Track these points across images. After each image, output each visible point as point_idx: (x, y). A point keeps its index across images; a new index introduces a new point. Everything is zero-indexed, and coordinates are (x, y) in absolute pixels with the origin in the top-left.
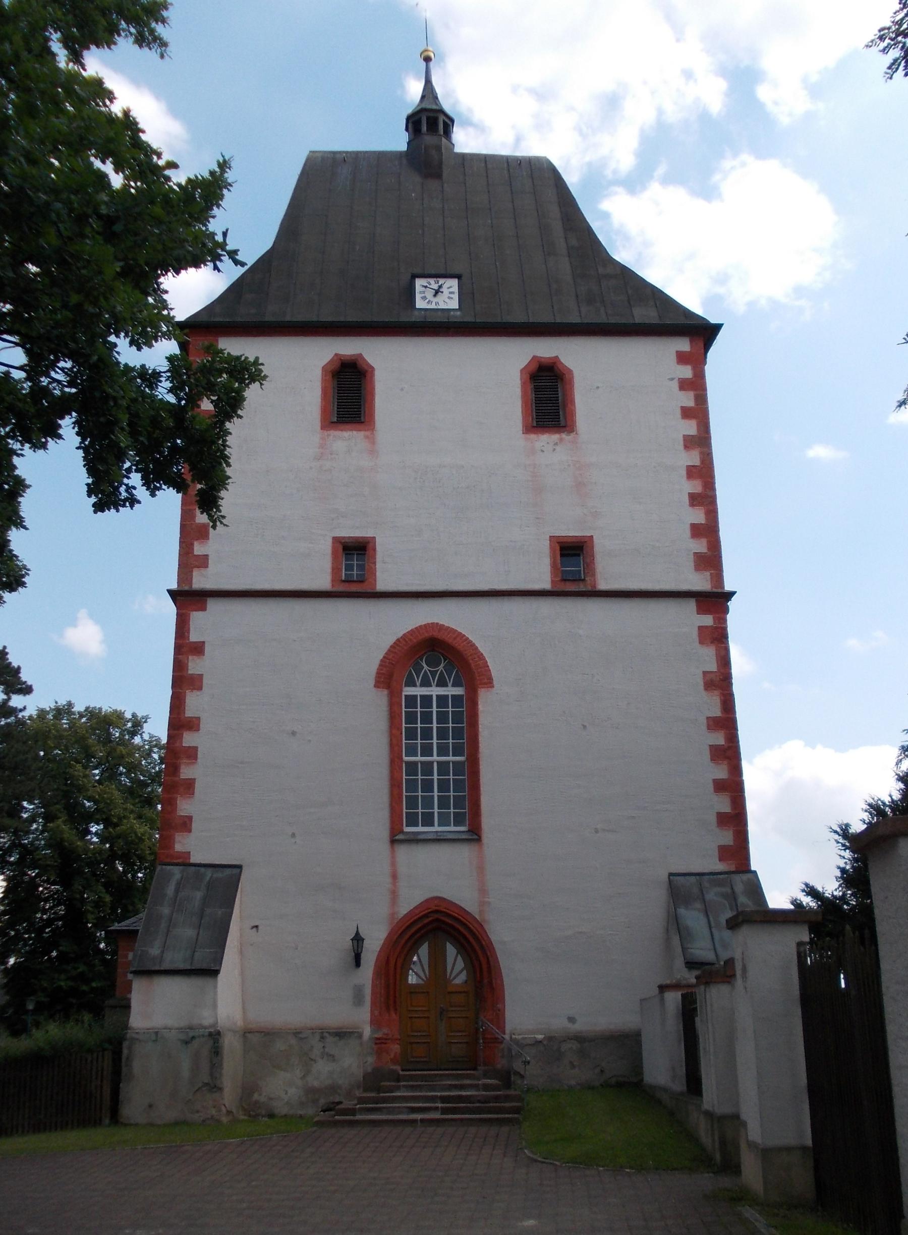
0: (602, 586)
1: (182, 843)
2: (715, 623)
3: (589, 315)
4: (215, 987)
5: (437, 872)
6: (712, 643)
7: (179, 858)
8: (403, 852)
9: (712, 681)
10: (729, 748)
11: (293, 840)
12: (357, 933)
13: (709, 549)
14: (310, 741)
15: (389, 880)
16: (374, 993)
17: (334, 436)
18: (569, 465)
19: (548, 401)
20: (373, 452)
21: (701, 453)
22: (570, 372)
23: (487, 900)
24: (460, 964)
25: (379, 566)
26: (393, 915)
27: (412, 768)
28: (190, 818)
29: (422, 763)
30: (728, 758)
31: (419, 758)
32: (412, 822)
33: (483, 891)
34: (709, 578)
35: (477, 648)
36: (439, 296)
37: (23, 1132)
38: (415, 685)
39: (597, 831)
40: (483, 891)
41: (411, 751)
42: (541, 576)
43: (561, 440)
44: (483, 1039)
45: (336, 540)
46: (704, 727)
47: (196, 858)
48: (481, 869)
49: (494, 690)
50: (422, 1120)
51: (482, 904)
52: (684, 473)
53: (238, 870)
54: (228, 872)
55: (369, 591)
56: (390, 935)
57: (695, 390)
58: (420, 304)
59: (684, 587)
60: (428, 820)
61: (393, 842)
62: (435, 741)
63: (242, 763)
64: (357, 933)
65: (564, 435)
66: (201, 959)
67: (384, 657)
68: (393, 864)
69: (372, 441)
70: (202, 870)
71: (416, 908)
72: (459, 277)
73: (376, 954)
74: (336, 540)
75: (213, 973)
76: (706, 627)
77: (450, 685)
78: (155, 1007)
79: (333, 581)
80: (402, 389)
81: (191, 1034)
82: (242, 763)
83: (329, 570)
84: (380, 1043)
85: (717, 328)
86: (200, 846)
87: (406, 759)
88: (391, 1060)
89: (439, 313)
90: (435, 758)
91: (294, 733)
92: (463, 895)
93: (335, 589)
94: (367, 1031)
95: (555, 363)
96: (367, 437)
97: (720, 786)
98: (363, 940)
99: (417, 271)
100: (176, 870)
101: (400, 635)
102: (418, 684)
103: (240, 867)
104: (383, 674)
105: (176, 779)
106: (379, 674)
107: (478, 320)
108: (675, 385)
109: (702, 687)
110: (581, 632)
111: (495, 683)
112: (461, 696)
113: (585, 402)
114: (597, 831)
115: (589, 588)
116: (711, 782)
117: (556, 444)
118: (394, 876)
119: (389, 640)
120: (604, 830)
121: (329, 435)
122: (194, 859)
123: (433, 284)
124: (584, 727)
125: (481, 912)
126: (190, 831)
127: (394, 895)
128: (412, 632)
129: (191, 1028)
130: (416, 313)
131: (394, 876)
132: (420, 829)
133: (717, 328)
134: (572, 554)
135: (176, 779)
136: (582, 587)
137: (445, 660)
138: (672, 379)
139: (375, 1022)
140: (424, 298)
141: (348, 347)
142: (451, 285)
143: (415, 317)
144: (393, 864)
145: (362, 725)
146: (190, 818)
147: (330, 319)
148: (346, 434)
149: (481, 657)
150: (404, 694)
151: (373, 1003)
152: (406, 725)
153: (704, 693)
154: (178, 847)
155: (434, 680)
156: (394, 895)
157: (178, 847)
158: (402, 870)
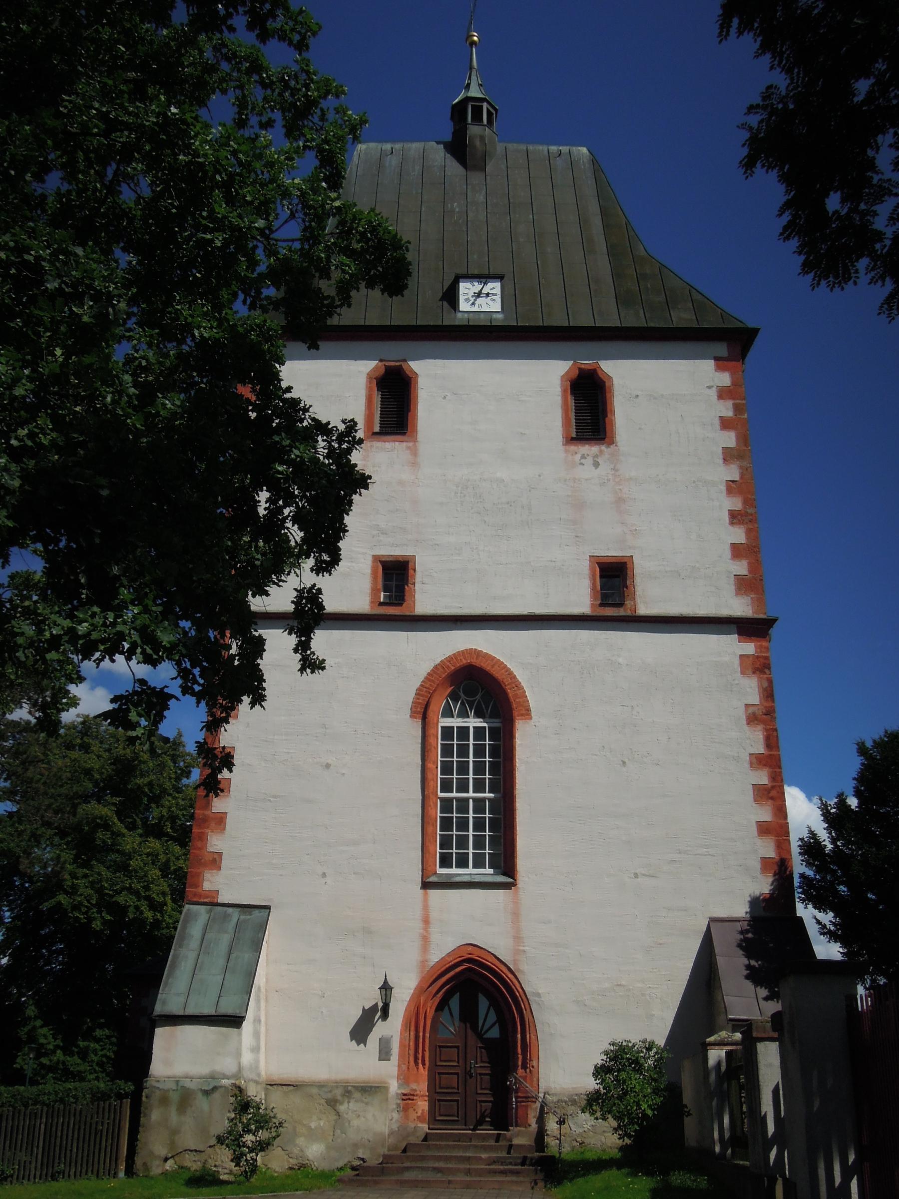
0: (643, 610)
1: (211, 881)
2: (756, 652)
3: (634, 319)
4: (240, 1034)
5: (471, 919)
6: (754, 673)
7: (207, 897)
8: (434, 893)
9: (754, 714)
10: (773, 787)
11: (323, 881)
12: (386, 982)
13: (750, 572)
14: (343, 774)
15: (421, 925)
16: (402, 1045)
17: (377, 447)
18: (609, 480)
19: (590, 413)
20: (414, 464)
21: (741, 467)
22: (610, 378)
23: (521, 948)
24: (492, 1017)
25: (418, 587)
26: (424, 962)
27: (447, 805)
28: (220, 854)
29: (475, 800)
30: (772, 798)
31: (454, 794)
32: (445, 861)
33: (518, 938)
34: (750, 602)
35: (515, 677)
36: (481, 300)
37: (35, 1182)
38: (453, 717)
39: (636, 876)
40: (518, 938)
41: (446, 786)
42: (580, 598)
43: (601, 452)
44: (516, 1098)
45: (376, 558)
46: (747, 765)
47: (224, 897)
48: (516, 915)
49: (532, 722)
50: (509, 1182)
51: (517, 952)
52: (723, 488)
53: (264, 913)
54: (256, 913)
55: (408, 613)
56: (421, 981)
57: (733, 399)
58: (464, 306)
59: (724, 612)
60: (462, 862)
61: (426, 885)
62: (471, 776)
63: (275, 797)
64: (386, 982)
65: (603, 448)
66: (227, 1007)
67: (421, 685)
68: (426, 907)
69: (415, 453)
70: (230, 910)
71: (448, 955)
72: (500, 277)
73: (406, 1004)
74: (376, 558)
75: (235, 1021)
76: (747, 656)
77: (487, 716)
78: (178, 1055)
79: (372, 602)
80: (445, 398)
81: (213, 1084)
82: (275, 797)
83: (369, 591)
84: (407, 1098)
85: (754, 332)
86: (228, 883)
87: (441, 795)
88: (418, 1117)
89: (482, 316)
90: (471, 794)
91: (328, 766)
92: (497, 942)
93: (375, 612)
94: (394, 1087)
95: (595, 370)
96: (408, 448)
97: (764, 829)
98: (391, 989)
99: (463, 271)
100: (203, 909)
101: (438, 661)
102: (456, 713)
103: (268, 908)
104: (419, 703)
105: (207, 813)
106: (415, 703)
107: (652, 325)
108: (713, 393)
109: (745, 722)
110: (620, 660)
111: (533, 714)
112: (499, 728)
113: (623, 413)
114: (636, 876)
115: (629, 613)
116: (754, 824)
117: (597, 456)
118: (426, 921)
119: (425, 668)
120: (644, 875)
121: (372, 446)
122: (221, 899)
123: (477, 287)
124: (624, 763)
125: (515, 962)
126: (219, 868)
127: (425, 940)
128: (450, 659)
129: (213, 1078)
130: (459, 315)
131: (426, 921)
132: (454, 871)
133: (754, 332)
134: (613, 577)
135: (207, 813)
136: (621, 612)
137: (482, 689)
138: (710, 387)
139: (404, 1077)
140: (467, 300)
141: (393, 351)
142: (494, 287)
143: (459, 319)
144: (426, 907)
145: (397, 758)
146: (220, 854)
147: (375, 323)
148: (388, 445)
149: (518, 685)
150: (440, 725)
151: (401, 1056)
152: (443, 761)
153: (746, 728)
154: (207, 886)
155: (487, 708)
156: (425, 940)
157: (207, 886)
158: (434, 915)
